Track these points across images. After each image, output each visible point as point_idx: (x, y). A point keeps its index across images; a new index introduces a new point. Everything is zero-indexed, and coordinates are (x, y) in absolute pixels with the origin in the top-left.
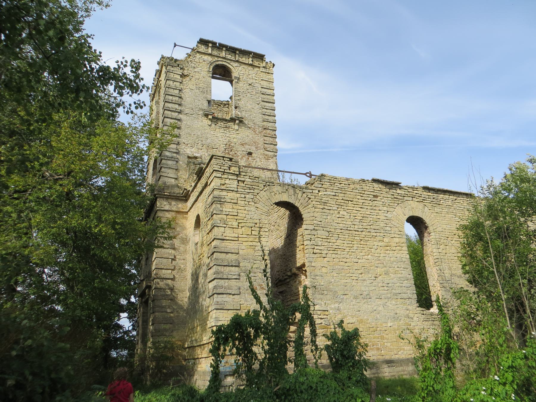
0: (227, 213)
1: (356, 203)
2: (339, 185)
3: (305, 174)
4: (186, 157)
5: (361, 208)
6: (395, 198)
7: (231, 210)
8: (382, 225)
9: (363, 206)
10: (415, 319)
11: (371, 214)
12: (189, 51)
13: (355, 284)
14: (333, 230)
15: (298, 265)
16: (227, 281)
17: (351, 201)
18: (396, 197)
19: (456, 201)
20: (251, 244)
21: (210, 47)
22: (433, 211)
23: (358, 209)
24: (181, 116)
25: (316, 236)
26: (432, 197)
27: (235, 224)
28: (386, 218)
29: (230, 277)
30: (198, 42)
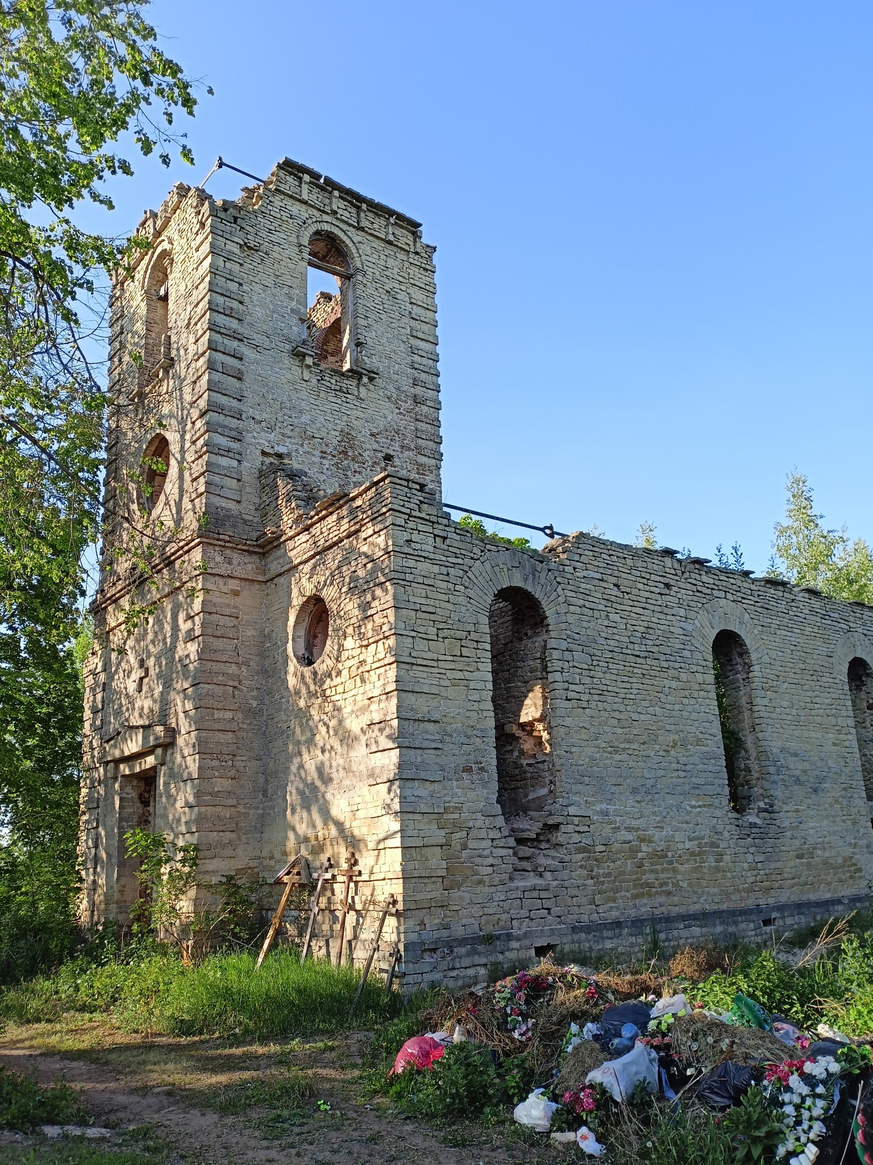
0: (418, 607)
1: (635, 598)
2: (608, 558)
3: (542, 530)
4: (258, 452)
5: (644, 608)
6: (698, 591)
7: (423, 601)
9: (647, 606)
10: (726, 834)
11: (660, 621)
12: (252, 184)
13: (634, 764)
14: (599, 653)
15: (523, 719)
16: (419, 752)
17: (628, 593)
18: (699, 588)
19: (793, 604)
20: (460, 675)
21: (306, 183)
22: (757, 622)
25: (571, 664)
26: (756, 593)
28: (684, 632)
29: (426, 744)
30: (280, 167)
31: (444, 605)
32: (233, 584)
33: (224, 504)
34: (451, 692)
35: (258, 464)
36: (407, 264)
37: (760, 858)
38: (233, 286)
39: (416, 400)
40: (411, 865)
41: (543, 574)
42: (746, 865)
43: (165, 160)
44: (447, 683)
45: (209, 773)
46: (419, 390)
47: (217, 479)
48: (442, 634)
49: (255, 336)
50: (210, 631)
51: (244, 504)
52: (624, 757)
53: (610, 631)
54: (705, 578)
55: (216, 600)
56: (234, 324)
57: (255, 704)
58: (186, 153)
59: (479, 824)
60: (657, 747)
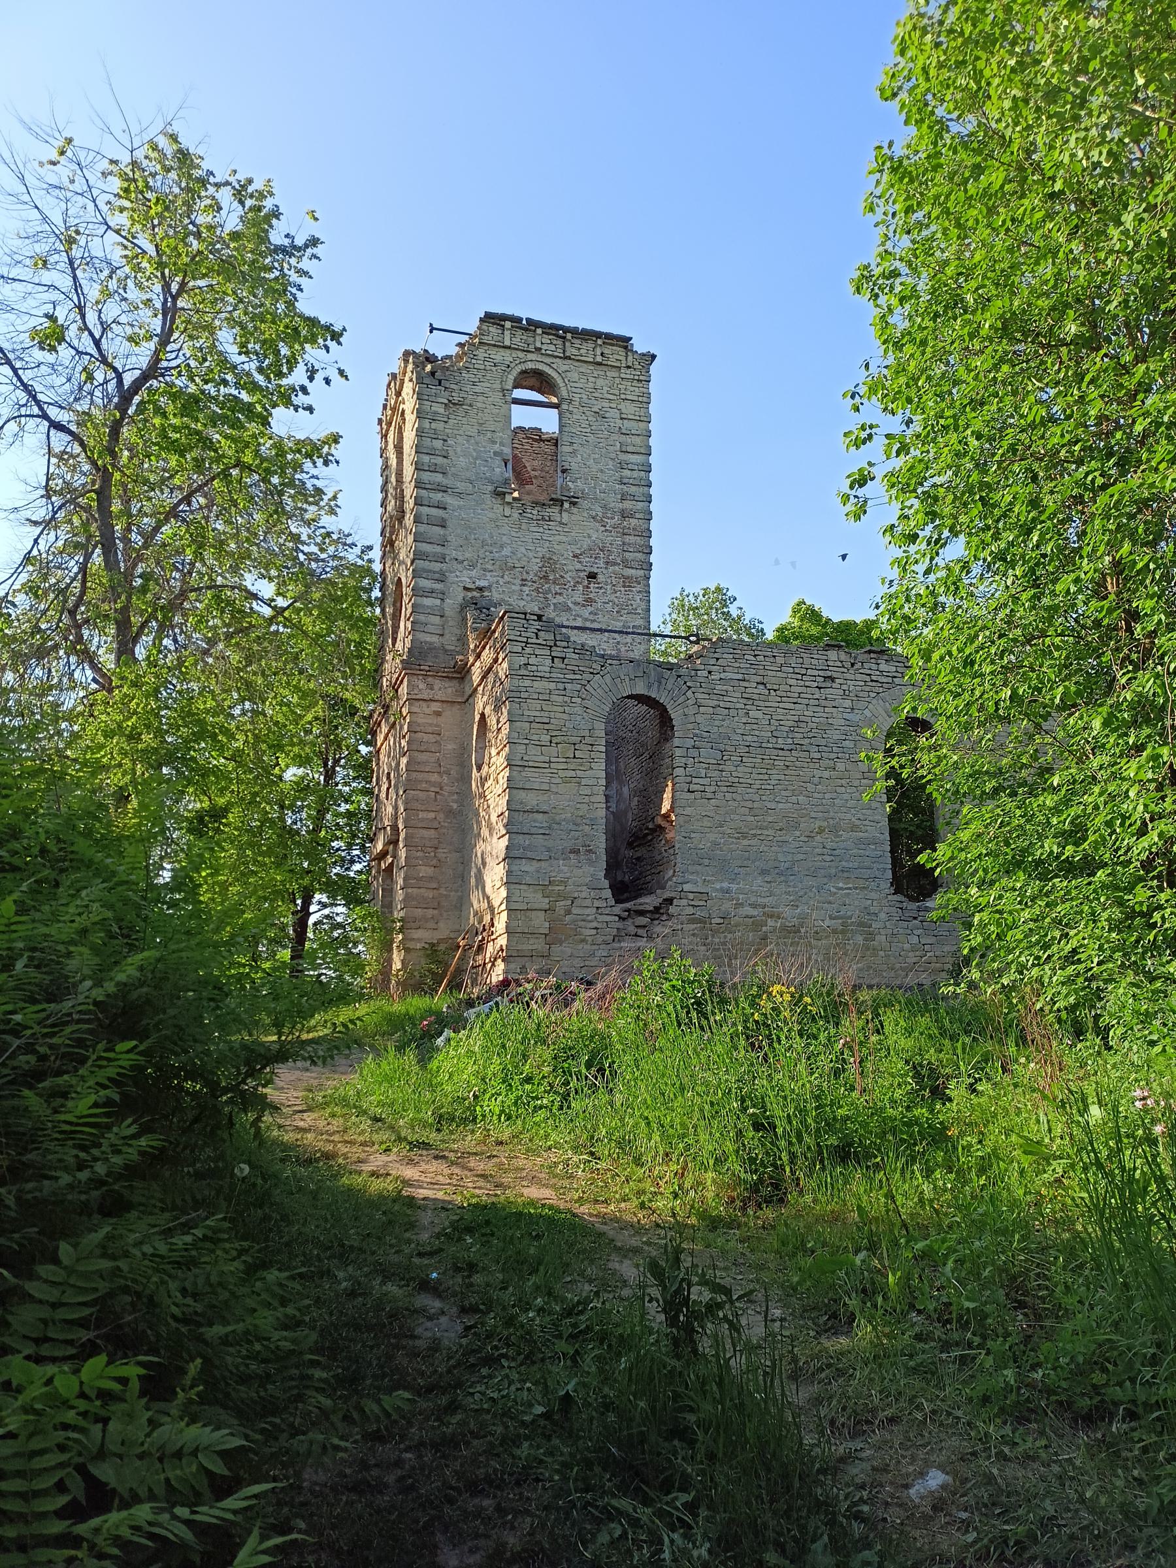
8: (836, 736)
10: (883, 916)
12: (463, 339)
20: (573, 774)
23: (787, 706)
24: (449, 500)
27: (545, 738)
29: (533, 831)
30: (481, 320)
31: (558, 715)
32: (435, 707)
33: (428, 638)
34: (562, 789)
35: (460, 599)
36: (618, 381)
37: (932, 940)
38: (438, 444)
39: (624, 515)
40: (515, 923)
41: (672, 680)
42: (907, 946)
43: (327, 381)
44: (558, 781)
45: (414, 862)
46: (628, 505)
47: (422, 618)
48: (555, 740)
49: (459, 484)
50: (414, 747)
51: (447, 636)
52: (754, 842)
53: (748, 727)
54: (883, 666)
55: (420, 721)
56: (438, 478)
57: (455, 806)
58: (341, 373)
59: (583, 895)
60: (798, 833)
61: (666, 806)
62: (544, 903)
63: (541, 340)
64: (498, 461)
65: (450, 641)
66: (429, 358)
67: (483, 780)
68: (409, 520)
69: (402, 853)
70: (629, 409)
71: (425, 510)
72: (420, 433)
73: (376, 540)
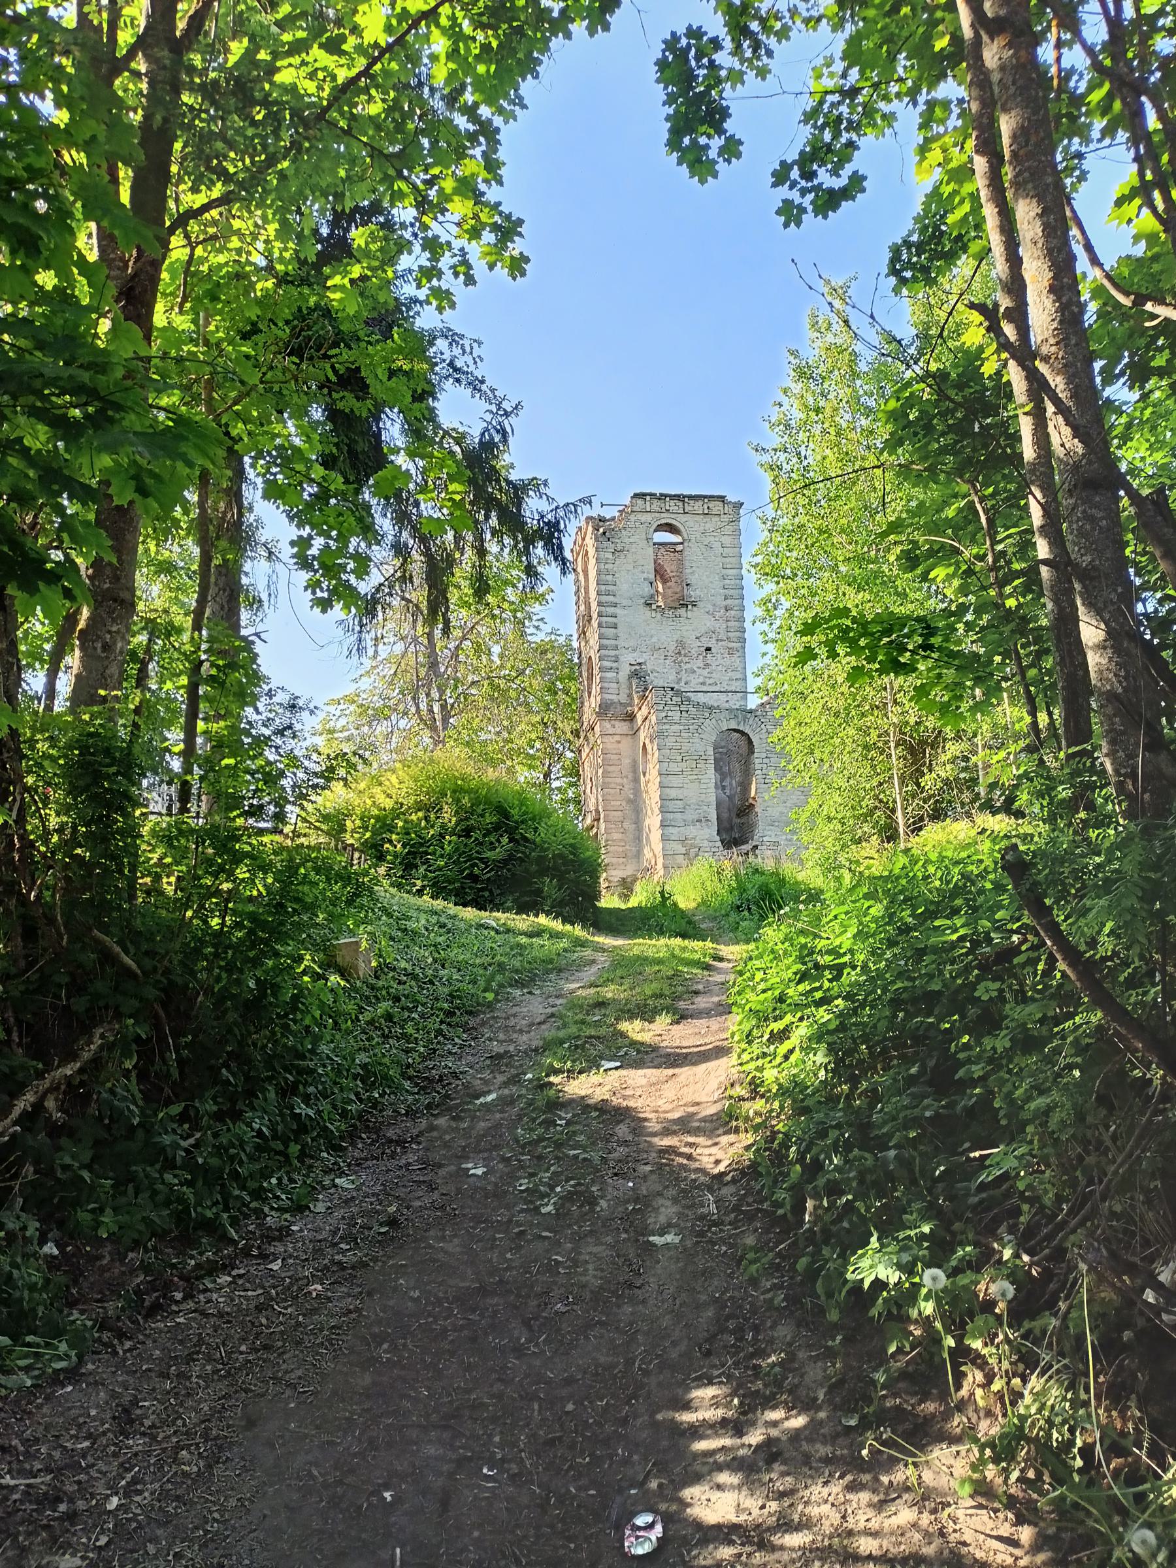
32: (617, 738)
38: (610, 578)
46: (729, 602)
56: (611, 598)
61: (753, 794)
62: (683, 851)
63: (671, 505)
64: (647, 584)
65: (623, 698)
66: (602, 520)
67: (647, 783)
68: (595, 623)
69: (603, 826)
70: (727, 540)
71: (604, 619)
72: (599, 572)
73: (573, 630)
